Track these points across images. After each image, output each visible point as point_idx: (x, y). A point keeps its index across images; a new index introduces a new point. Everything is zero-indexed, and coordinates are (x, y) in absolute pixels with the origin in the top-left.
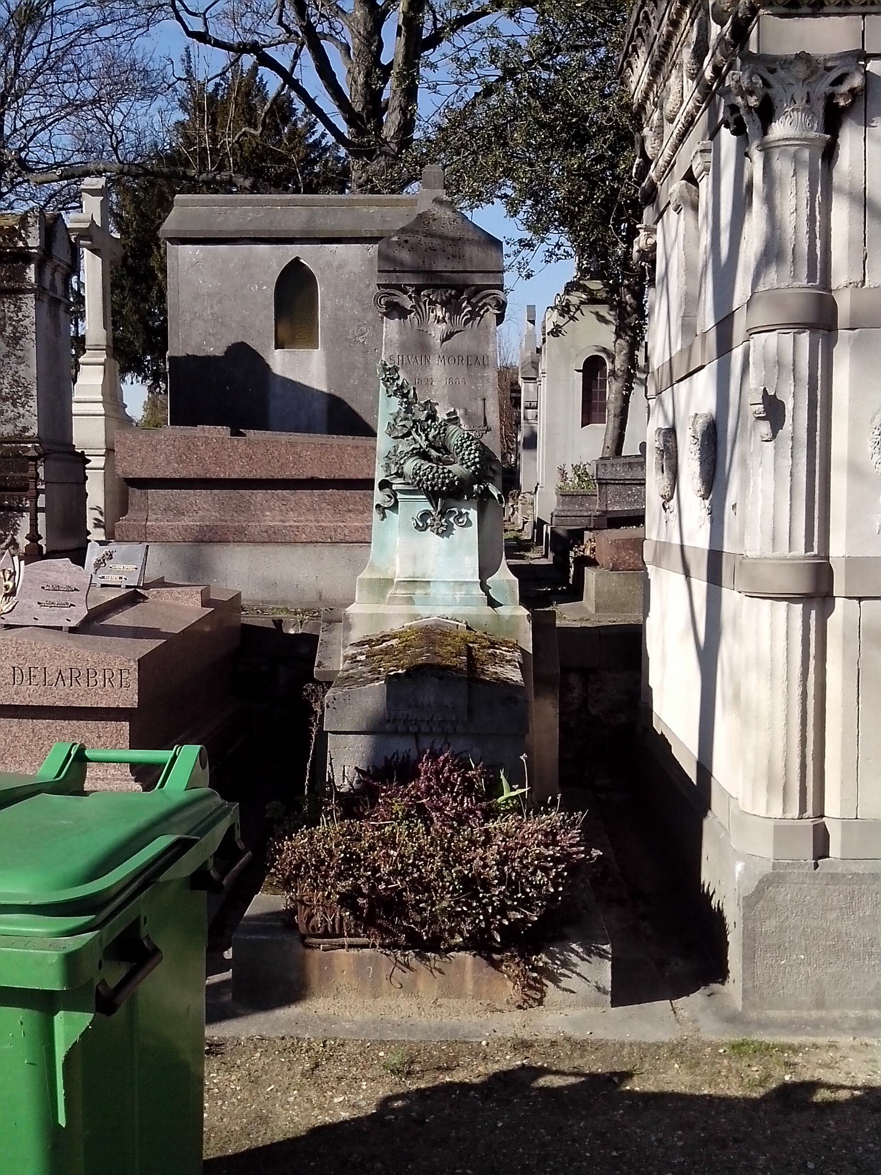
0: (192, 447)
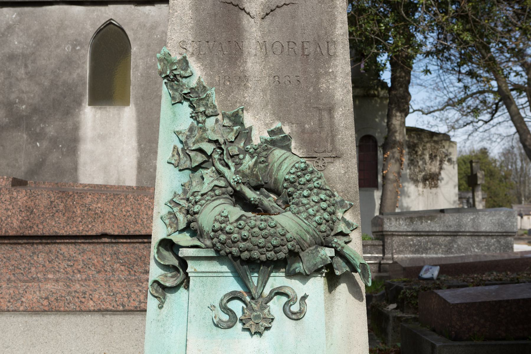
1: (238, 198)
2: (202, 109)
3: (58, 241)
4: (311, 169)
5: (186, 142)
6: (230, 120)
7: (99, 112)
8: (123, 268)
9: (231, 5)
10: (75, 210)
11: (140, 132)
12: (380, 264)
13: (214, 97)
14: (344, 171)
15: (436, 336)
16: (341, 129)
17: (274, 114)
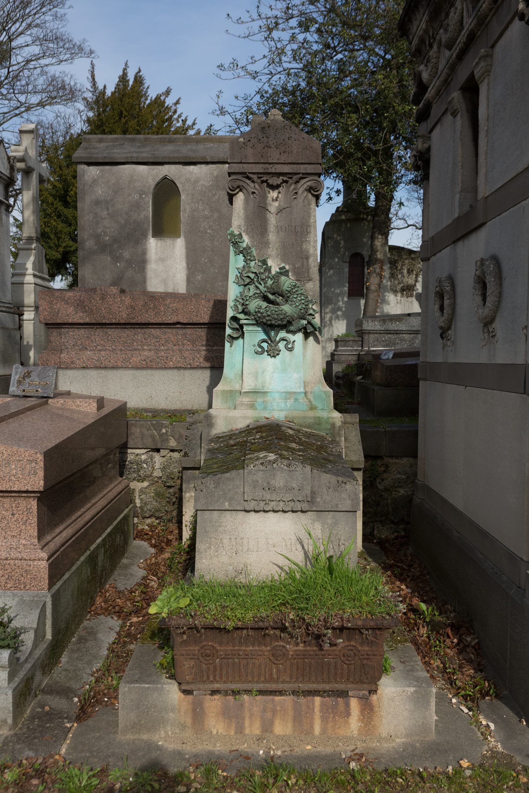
0: (93, 301)
1: (265, 299)
2: (249, 258)
7: (159, 242)
12: (359, 355)
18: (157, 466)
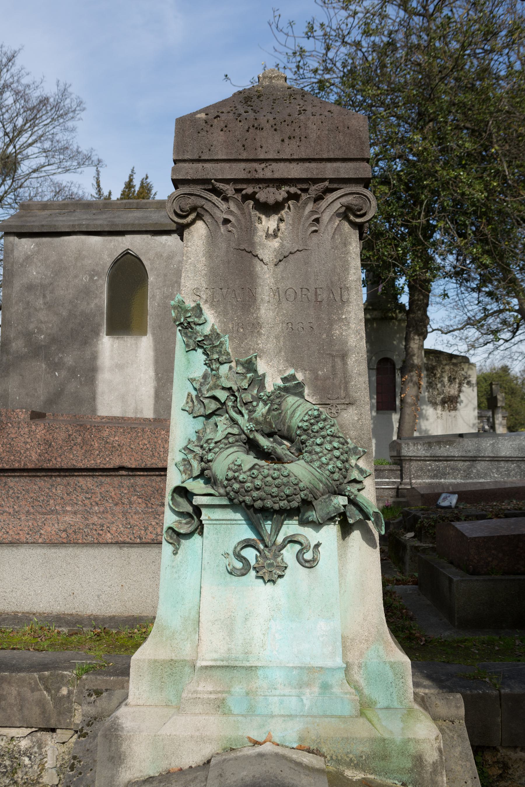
1: (252, 446)
2: (216, 356)
3: (76, 474)
4: (324, 417)
5: (200, 389)
6: (244, 367)
7: (117, 341)
8: (140, 500)
9: (244, 252)
10: (93, 443)
11: (157, 362)
12: (398, 489)
13: (227, 344)
14: (358, 417)
15: (454, 569)
16: (354, 375)
17: (287, 361)
18: (50, 762)
